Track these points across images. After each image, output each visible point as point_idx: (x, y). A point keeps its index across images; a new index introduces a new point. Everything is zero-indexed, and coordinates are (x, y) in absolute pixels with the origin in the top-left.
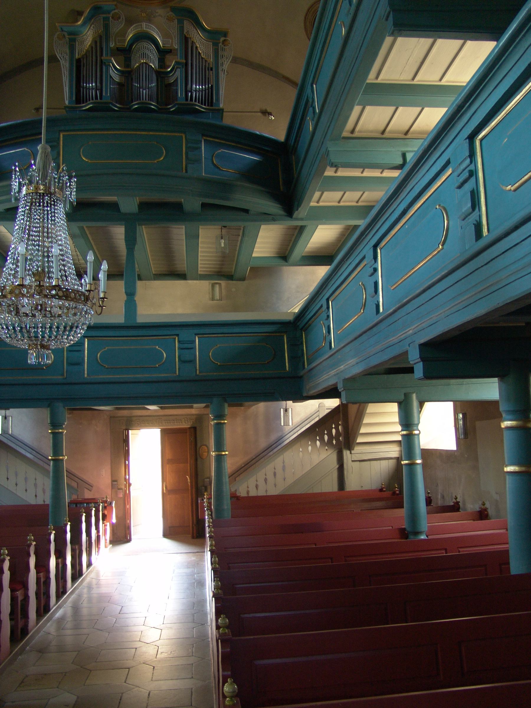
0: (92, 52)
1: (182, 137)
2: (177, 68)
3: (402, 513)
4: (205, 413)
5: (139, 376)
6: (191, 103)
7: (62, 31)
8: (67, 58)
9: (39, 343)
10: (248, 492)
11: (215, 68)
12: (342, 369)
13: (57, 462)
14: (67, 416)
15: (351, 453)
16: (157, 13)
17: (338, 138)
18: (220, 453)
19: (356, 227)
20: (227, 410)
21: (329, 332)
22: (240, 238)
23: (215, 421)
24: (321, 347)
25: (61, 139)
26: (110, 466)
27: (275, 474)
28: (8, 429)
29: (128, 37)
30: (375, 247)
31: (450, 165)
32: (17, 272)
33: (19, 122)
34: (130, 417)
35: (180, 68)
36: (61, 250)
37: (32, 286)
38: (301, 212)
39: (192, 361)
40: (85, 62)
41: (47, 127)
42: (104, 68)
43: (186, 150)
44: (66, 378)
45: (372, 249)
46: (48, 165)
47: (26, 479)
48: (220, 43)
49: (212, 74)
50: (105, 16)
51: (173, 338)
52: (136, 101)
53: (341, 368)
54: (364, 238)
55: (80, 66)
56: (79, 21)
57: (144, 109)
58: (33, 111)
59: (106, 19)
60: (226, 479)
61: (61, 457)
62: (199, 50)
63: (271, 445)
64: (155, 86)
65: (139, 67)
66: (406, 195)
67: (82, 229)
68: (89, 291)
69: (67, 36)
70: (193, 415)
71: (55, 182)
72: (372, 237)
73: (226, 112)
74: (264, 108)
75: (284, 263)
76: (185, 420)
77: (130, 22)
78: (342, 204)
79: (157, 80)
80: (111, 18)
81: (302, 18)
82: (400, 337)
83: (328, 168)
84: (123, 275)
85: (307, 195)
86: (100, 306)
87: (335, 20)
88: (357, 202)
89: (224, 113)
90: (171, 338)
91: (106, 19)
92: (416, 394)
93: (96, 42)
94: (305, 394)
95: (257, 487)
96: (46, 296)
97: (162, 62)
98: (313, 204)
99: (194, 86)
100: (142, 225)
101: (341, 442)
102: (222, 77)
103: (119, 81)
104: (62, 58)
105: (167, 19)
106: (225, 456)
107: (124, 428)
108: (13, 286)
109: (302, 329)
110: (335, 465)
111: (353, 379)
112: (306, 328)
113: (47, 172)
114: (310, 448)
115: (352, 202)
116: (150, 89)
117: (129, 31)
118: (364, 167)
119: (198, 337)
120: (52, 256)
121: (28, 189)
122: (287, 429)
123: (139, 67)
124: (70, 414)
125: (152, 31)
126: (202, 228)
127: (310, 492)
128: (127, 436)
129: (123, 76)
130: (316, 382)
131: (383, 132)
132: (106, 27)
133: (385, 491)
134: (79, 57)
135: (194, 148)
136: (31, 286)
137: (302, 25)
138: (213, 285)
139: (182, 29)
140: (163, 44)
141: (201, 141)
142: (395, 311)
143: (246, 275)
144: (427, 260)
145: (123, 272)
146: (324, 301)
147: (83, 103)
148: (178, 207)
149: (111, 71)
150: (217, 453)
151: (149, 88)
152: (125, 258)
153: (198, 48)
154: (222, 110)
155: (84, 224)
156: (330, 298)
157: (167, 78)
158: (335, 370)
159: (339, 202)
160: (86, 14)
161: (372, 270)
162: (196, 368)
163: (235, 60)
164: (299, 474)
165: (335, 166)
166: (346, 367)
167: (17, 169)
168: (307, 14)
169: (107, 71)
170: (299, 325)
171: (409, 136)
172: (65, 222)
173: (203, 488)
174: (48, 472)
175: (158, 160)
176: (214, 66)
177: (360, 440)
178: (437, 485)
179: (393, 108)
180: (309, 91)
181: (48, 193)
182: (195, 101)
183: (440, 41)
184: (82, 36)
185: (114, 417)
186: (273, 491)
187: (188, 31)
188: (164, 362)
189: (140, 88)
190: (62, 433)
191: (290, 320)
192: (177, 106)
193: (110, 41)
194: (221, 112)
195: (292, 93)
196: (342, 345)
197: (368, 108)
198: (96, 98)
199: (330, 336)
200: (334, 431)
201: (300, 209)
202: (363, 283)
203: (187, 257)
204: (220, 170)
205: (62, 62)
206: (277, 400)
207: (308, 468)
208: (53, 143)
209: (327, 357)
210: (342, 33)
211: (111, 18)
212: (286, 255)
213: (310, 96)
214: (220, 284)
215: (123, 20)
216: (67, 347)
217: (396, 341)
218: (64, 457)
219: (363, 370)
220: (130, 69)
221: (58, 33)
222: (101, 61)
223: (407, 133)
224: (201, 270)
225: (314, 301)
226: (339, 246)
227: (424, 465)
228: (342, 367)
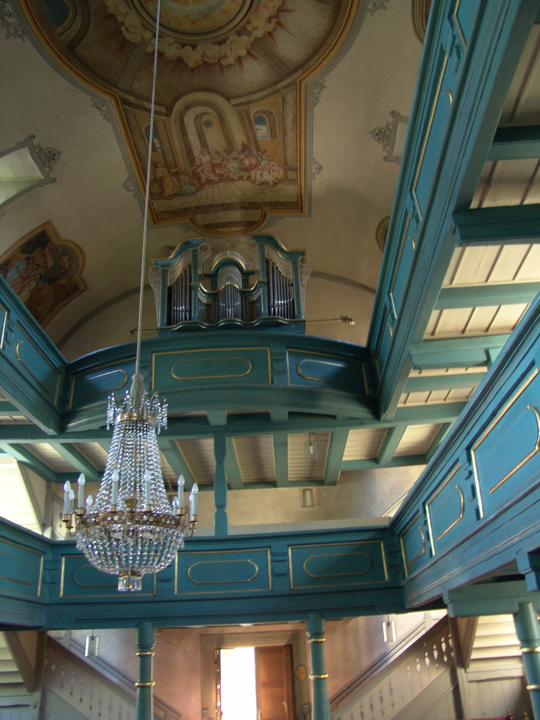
0: (182, 279)
1: (267, 350)
2: (260, 287)
4: (302, 628)
5: (230, 592)
6: (274, 317)
7: (156, 264)
8: (160, 286)
9: (130, 569)
11: (295, 284)
12: (445, 580)
13: (144, 689)
14: (156, 634)
15: (466, 672)
16: (240, 241)
17: (420, 342)
18: (319, 676)
19: (446, 426)
20: (325, 625)
21: (428, 538)
22: (329, 443)
23: (312, 640)
24: (421, 554)
25: (154, 359)
27: (381, 699)
28: (94, 651)
29: (214, 264)
30: (468, 449)
31: (535, 366)
32: (110, 498)
33: (115, 346)
34: (223, 635)
35: (262, 287)
36: (153, 474)
37: (124, 513)
38: (389, 414)
39: (285, 574)
40: (176, 288)
41: (142, 349)
42: (193, 292)
43: (271, 362)
44: (155, 596)
45: (465, 452)
46: (141, 393)
47: (110, 708)
48: (298, 261)
49: (292, 290)
50: (193, 248)
51: (265, 550)
52: (222, 319)
53: (445, 578)
54: (455, 441)
55: (171, 292)
56: (171, 255)
57: (231, 326)
58: (128, 333)
60: (327, 707)
61: (148, 684)
62: (280, 270)
63: (375, 663)
64: (240, 304)
65: (224, 289)
66: (494, 397)
67: (172, 442)
68: (180, 515)
69: (160, 269)
70: (288, 631)
71: (147, 410)
72: (464, 439)
73: (308, 321)
74: (344, 315)
75: (376, 465)
76: (280, 637)
77: (216, 250)
78: (429, 403)
79: (242, 299)
80: (199, 250)
81: (374, 233)
82: (506, 545)
83: (412, 370)
84: (213, 485)
85: (393, 397)
86: (190, 529)
87: (404, 236)
88: (445, 399)
89: (306, 323)
90: (263, 551)
91: (195, 252)
92: (533, 603)
93: (186, 271)
94: (408, 606)
96: (138, 522)
97: (246, 283)
98: (400, 405)
99: (276, 302)
100: (230, 436)
101: (453, 658)
102: (303, 291)
103: (206, 302)
104: (155, 287)
105: (249, 246)
106: (325, 680)
107: (215, 647)
108: (106, 513)
109: (399, 535)
111: (459, 590)
112: (404, 533)
113: (140, 401)
114: (418, 666)
115: (439, 400)
116: (235, 308)
118: (447, 367)
119: (291, 549)
120: (144, 481)
121: (122, 417)
122: (391, 645)
123: (225, 289)
124: (158, 632)
125: (236, 258)
126: (290, 436)
128: (219, 656)
129: (210, 298)
130: (421, 592)
131: (464, 331)
132: (195, 257)
134: (171, 284)
135: (279, 360)
136: (122, 513)
137: (374, 239)
138: (304, 492)
139: (263, 253)
140: (246, 267)
141: (285, 353)
142: (497, 517)
143: (337, 479)
144: (524, 462)
145: (213, 482)
146: (419, 506)
147: (174, 324)
148: (265, 417)
149: (199, 295)
150: (315, 676)
151: (234, 307)
152: (214, 468)
153: (279, 268)
154: (304, 321)
155: (175, 438)
156: (426, 502)
157: (250, 296)
158: (438, 581)
159: (426, 401)
160: (177, 249)
161: (466, 473)
162: (290, 581)
163: (314, 274)
164: (409, 699)
165: (419, 368)
166: (450, 577)
167: (113, 399)
168: (378, 229)
169: (196, 295)
170: (395, 531)
171: (490, 332)
172: (156, 446)
173: (302, 716)
174: (134, 699)
175: (244, 374)
176: (295, 297)
177: (474, 655)
179: (469, 310)
180: (386, 299)
181: (141, 420)
182: (278, 315)
183: (507, 248)
184: (173, 267)
185: (205, 635)
187: (269, 254)
188: (255, 577)
189: (226, 307)
190: (150, 655)
191: (386, 526)
192: (261, 321)
193: (198, 267)
194: (303, 323)
195: (372, 299)
196: (444, 553)
197: (446, 312)
198: (186, 319)
199: (429, 543)
200: (444, 646)
201: (387, 412)
202: (459, 486)
203: (276, 465)
204: (305, 378)
205: (155, 290)
206: (378, 613)
207: (418, 691)
208: (145, 366)
209: (428, 565)
210: (413, 247)
211: (199, 250)
214: (311, 490)
215: (210, 251)
216: (158, 573)
217: (502, 548)
218: (151, 684)
219: (469, 580)
220: (216, 292)
221: (152, 267)
222: (191, 287)
223: (487, 329)
224: (292, 474)
225: (409, 507)
226: (430, 444)
228: (446, 576)
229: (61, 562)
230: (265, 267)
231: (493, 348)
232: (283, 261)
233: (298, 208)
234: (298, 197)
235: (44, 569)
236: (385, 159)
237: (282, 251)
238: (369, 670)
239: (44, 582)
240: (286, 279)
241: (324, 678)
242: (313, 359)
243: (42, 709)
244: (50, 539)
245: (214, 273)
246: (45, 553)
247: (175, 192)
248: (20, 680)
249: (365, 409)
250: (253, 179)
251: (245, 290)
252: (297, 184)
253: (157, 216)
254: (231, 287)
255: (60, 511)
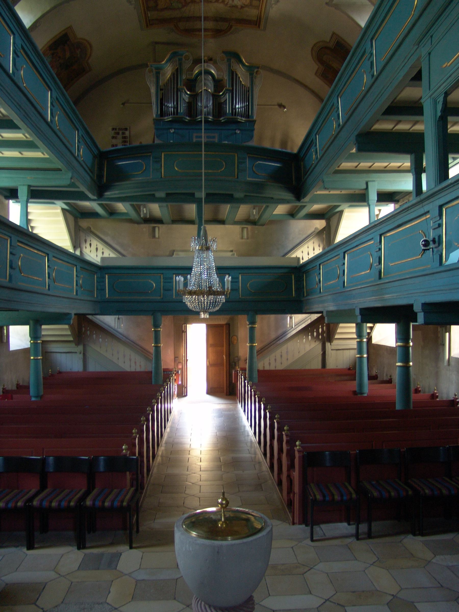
3: (356, 383)
7: (151, 66)
10: (264, 367)
15: (331, 344)
18: (252, 344)
23: (250, 326)
26: (173, 348)
27: (281, 356)
29: (194, 72)
39: (237, 290)
44: (163, 299)
58: (121, 106)
59: (180, 60)
61: (159, 345)
91: (180, 60)
94: (304, 311)
95: (270, 364)
101: (325, 337)
110: (320, 352)
114: (304, 340)
117: (195, 68)
119: (241, 275)
127: (304, 368)
133: (352, 370)
138: (243, 229)
139: (230, 65)
140: (217, 76)
147: (165, 116)
150: (250, 344)
153: (240, 78)
162: (239, 294)
173: (234, 363)
177: (337, 336)
178: (384, 368)
186: (280, 367)
200: (320, 330)
207: (302, 353)
212: (294, 212)
213: (314, 139)
214: (247, 228)
220: (195, 93)
222: (177, 89)
227: (368, 358)
229: (105, 278)
230: (231, 78)
231: (371, 181)
232: (243, 72)
233: (256, 25)
234: (258, 18)
235: (97, 282)
236: (327, 4)
237: (243, 64)
238: (274, 340)
239: (97, 289)
240: (245, 86)
241: (255, 346)
242: (264, 161)
243: (84, 355)
244: (19, 226)
245: (194, 79)
246: (97, 273)
247: (166, 7)
248: (71, 339)
249: (291, 195)
250: (226, 3)
251: (216, 94)
252: (258, 9)
253: (150, 22)
254: (206, 92)
255: (85, 238)
